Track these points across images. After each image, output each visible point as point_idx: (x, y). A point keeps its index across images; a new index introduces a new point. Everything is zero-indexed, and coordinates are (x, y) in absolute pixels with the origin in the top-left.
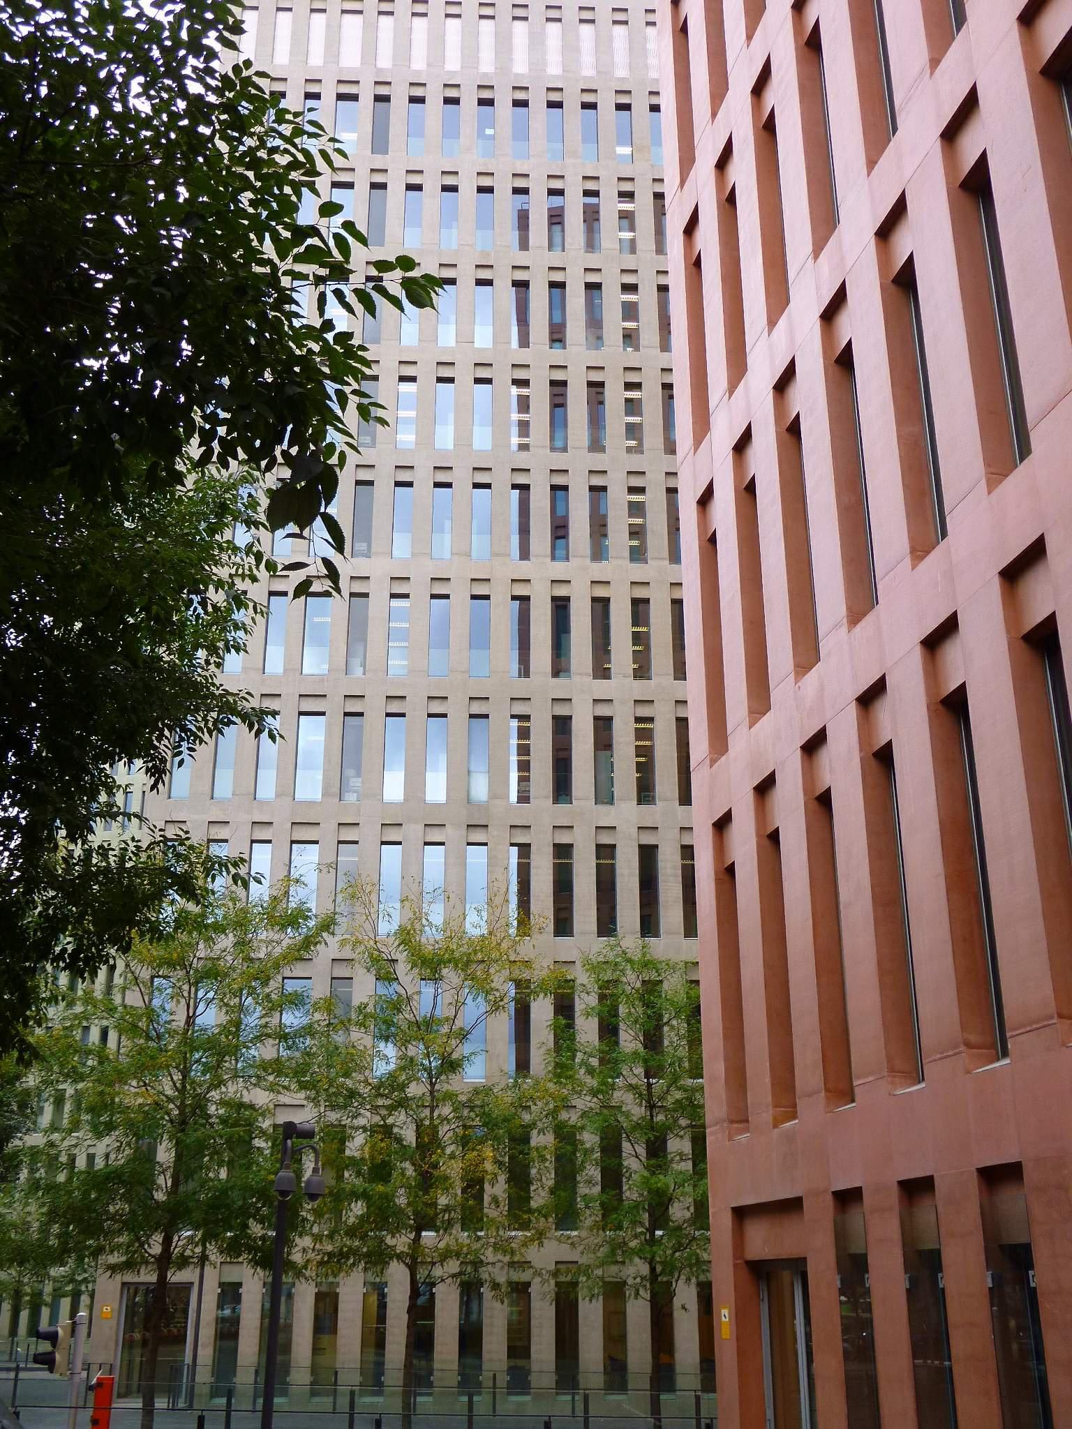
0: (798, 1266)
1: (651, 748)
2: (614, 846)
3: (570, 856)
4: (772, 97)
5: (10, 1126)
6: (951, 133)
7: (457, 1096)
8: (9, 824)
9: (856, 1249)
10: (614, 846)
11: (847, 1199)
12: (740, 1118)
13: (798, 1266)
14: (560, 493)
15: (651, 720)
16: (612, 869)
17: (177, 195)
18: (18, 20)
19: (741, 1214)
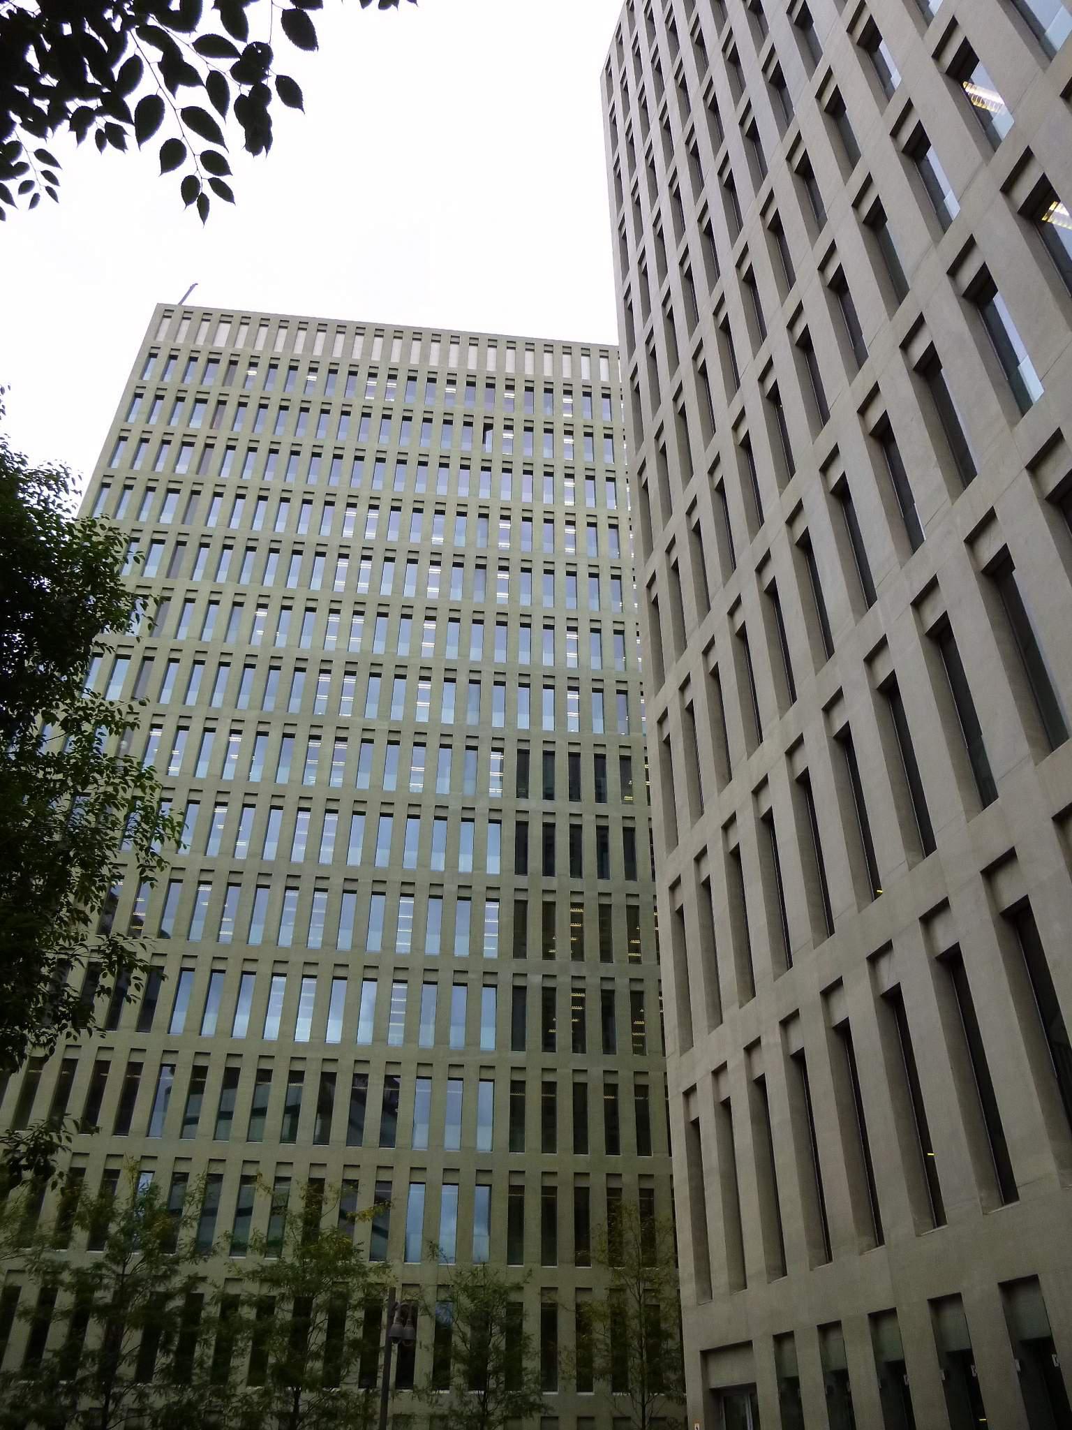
0: (750, 1389)
1: (583, 1012)
2: (524, 1082)
3: (554, 1091)
4: (646, 474)
5: (24, 1378)
6: (760, 570)
7: (506, 1292)
8: (489, 1429)
9: (790, 1374)
10: (524, 1082)
11: (781, 1339)
12: (706, 1289)
13: (750, 1389)
14: (549, 757)
15: (583, 991)
16: (553, 1100)
17: (39, 109)
18: (80, 1419)
19: (706, 1355)
